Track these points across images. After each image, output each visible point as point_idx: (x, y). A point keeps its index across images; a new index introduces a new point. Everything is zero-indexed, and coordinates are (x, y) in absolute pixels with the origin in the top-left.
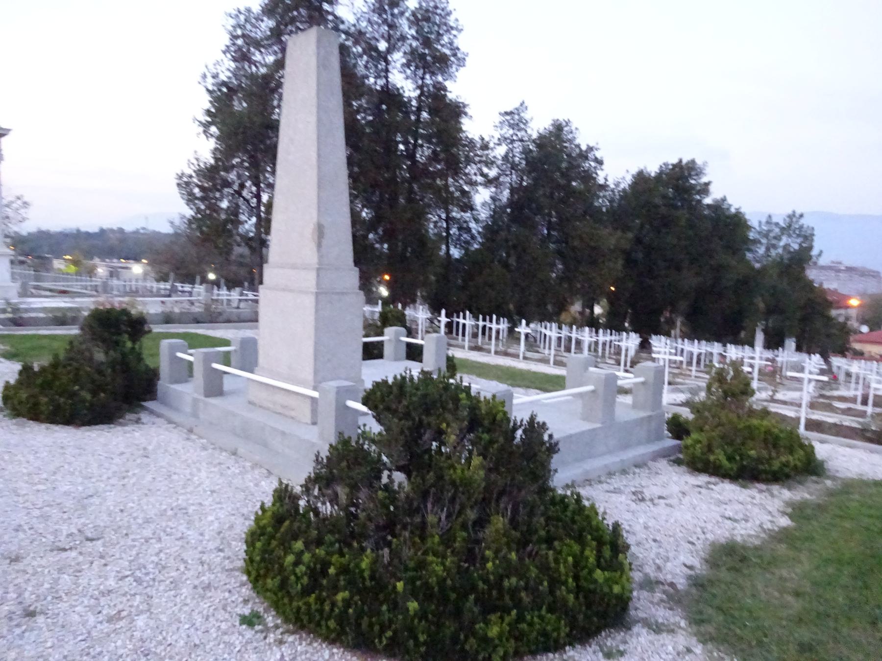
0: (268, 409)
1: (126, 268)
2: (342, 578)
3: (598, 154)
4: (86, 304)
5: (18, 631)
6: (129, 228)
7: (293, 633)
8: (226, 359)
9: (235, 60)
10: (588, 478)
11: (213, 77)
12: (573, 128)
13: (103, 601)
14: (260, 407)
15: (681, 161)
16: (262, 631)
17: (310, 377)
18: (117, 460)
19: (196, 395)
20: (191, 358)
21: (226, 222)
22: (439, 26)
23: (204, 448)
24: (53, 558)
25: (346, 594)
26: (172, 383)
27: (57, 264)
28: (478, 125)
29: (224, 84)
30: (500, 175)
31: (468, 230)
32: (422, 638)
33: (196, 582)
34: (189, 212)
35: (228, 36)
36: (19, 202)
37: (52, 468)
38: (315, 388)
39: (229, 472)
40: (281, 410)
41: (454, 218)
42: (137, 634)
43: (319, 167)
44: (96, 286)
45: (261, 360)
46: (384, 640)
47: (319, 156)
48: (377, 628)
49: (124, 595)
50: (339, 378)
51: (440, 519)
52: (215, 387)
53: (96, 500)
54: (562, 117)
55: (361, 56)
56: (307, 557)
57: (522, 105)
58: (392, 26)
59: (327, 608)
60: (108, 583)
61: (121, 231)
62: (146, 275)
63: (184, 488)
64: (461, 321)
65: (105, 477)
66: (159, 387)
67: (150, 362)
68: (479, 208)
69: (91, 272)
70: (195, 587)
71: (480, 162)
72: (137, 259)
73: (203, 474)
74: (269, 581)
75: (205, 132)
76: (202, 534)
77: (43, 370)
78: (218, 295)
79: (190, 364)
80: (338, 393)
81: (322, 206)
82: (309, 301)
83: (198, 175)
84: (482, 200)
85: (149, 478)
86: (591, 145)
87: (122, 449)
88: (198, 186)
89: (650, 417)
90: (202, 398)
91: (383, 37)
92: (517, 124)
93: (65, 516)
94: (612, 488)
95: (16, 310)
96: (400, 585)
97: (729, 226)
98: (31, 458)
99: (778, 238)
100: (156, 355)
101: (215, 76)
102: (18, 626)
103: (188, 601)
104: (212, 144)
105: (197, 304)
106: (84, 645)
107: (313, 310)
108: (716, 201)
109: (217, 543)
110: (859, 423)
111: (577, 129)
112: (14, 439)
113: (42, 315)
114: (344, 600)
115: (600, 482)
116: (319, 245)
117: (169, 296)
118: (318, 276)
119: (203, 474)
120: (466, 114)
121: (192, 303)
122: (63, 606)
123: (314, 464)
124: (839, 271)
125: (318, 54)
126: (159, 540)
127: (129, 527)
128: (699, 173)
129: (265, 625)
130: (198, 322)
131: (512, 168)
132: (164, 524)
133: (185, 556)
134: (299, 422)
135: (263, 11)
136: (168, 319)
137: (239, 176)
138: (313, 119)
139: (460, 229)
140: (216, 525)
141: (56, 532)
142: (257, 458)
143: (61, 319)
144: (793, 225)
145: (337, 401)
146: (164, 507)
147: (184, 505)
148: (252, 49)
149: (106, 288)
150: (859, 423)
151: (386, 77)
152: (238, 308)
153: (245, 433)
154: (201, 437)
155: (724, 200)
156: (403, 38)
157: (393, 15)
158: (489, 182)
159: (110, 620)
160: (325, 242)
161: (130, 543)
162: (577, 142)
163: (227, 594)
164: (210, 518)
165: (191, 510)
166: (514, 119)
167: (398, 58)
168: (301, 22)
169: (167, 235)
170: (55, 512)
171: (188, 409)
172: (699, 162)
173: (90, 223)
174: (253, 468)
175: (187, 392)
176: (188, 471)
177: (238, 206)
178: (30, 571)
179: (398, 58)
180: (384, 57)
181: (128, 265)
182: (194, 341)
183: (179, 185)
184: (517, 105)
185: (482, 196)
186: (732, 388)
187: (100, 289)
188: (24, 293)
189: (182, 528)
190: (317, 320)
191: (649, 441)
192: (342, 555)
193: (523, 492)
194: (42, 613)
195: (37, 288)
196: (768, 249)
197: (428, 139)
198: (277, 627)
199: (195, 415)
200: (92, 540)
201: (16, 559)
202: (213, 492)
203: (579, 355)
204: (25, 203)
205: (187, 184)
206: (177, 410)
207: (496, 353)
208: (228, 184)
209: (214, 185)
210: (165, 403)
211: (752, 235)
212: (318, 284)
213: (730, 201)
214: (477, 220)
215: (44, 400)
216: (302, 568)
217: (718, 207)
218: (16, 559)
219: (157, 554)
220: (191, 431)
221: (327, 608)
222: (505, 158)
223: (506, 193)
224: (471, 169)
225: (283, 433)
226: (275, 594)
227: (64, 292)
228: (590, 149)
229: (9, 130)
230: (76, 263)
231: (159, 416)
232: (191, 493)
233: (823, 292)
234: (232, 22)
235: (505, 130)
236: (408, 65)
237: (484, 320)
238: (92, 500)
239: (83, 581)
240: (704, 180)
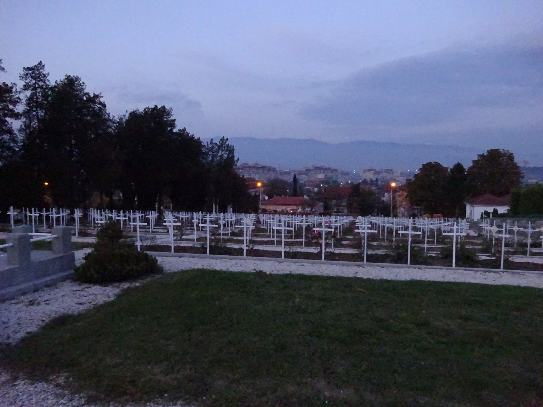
3: (102, 100)
12: (81, 82)
15: (156, 107)
54: (73, 74)
57: (39, 64)
64: (29, 214)
68: (16, 132)
86: (97, 94)
89: (62, 257)
92: (39, 77)
97: (188, 144)
99: (218, 151)
108: (180, 130)
110: (434, 254)
111: (83, 83)
124: (259, 168)
128: (168, 114)
144: (223, 144)
150: (434, 254)
155: (184, 130)
158: (17, 116)
162: (86, 91)
166: (35, 73)
172: (168, 107)
186: (112, 233)
191: (61, 270)
196: (213, 158)
203: (58, 227)
211: (204, 150)
213: (188, 131)
217: (183, 134)
222: (30, 99)
228: (96, 96)
233: (243, 179)
240: (172, 118)
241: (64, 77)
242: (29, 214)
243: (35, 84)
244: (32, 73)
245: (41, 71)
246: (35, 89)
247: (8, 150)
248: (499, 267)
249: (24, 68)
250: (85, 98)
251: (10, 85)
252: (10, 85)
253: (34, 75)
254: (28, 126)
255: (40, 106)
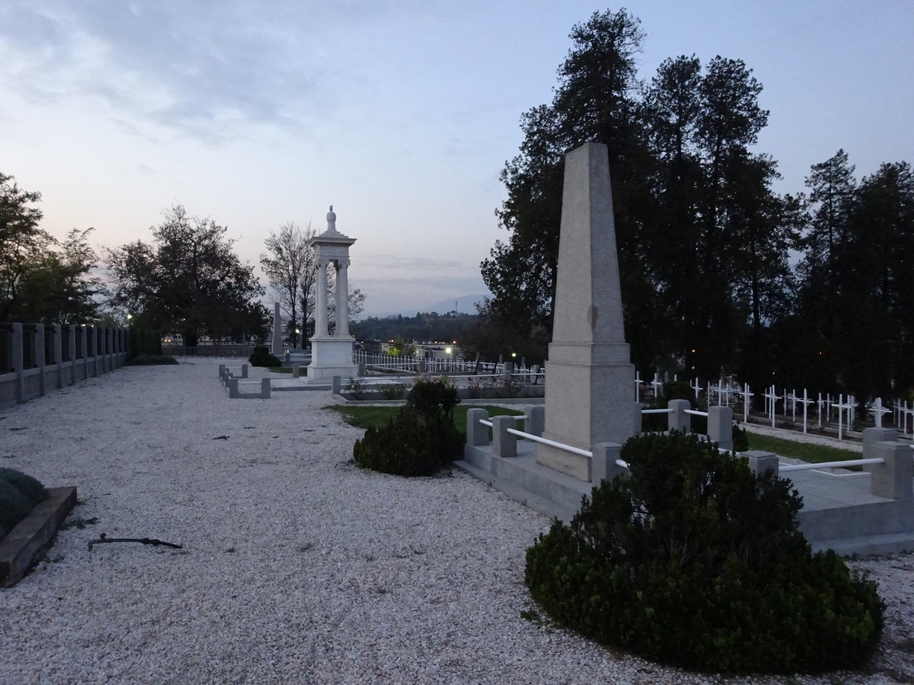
0: (553, 469)
1: (439, 349)
2: (595, 585)
4: (409, 381)
5: (375, 600)
6: (441, 312)
7: (558, 628)
8: (520, 426)
9: (531, 154)
10: (874, 553)
11: (513, 173)
13: (427, 591)
14: (547, 466)
16: (537, 624)
17: (587, 439)
18: (435, 502)
19: (495, 456)
20: (491, 424)
21: (526, 302)
22: (734, 90)
23: (500, 498)
24: (394, 561)
25: (598, 597)
26: (476, 445)
27: (385, 348)
28: (789, 182)
29: (522, 177)
30: (816, 234)
31: (781, 296)
32: (657, 638)
33: (491, 588)
34: (492, 297)
35: (524, 135)
36: (357, 296)
37: (390, 503)
38: (591, 450)
39: (520, 518)
40: (562, 469)
41: (763, 284)
42: (450, 612)
43: (592, 260)
44: (415, 366)
45: (548, 425)
46: (627, 636)
47: (592, 248)
48: (621, 626)
49: (442, 589)
50: (612, 441)
51: (681, 552)
52: (510, 448)
53: (421, 528)
55: (652, 132)
56: (570, 568)
57: (839, 155)
58: (683, 98)
59: (584, 607)
60: (430, 580)
61: (434, 315)
62: (455, 353)
63: (484, 525)
65: (426, 513)
66: (466, 450)
67: (459, 429)
68: (793, 271)
69: (411, 353)
70: (490, 590)
71: (788, 223)
72: (449, 342)
73: (499, 518)
74: (542, 586)
75: (505, 222)
76: (496, 558)
77: (382, 431)
78: (519, 372)
79: (490, 428)
80: (608, 452)
81: (595, 292)
82: (586, 373)
83: (499, 262)
84: (796, 262)
85: (459, 516)
87: (438, 495)
88: (499, 271)
90: (499, 457)
91: (674, 110)
93: (401, 536)
94: (901, 565)
95: (357, 387)
96: (640, 594)
98: (376, 496)
100: (465, 424)
101: (515, 172)
102: (375, 597)
103: (485, 598)
104: (512, 232)
105: (499, 381)
106: (415, 613)
107: (589, 381)
109: (508, 565)
112: (363, 483)
113: (375, 391)
114: (596, 601)
115: (889, 559)
116: (594, 325)
117: (475, 373)
118: (593, 351)
119: (499, 518)
120: (773, 172)
121: (494, 379)
122: (402, 590)
123: (580, 505)
125: (590, 165)
126: (465, 558)
127: (444, 548)
129: (540, 621)
130: (500, 397)
131: (831, 225)
132: (469, 548)
133: (483, 570)
134: (579, 480)
135: (555, 107)
136: (474, 394)
137: (537, 260)
138: (587, 218)
139: (769, 296)
140: (507, 554)
141: (395, 546)
142: (543, 508)
143: (390, 393)
145: (608, 461)
146: (469, 537)
147: (484, 537)
148: (547, 143)
149: (423, 368)
151: (679, 149)
152: (535, 384)
153: (534, 487)
154: (498, 490)
156: (695, 109)
157: (683, 87)
158: (799, 244)
159: (432, 602)
160: (599, 322)
161: (444, 558)
163: (513, 598)
164: (503, 548)
165: (488, 541)
167: (690, 128)
168: (591, 111)
169: (474, 316)
170: (394, 533)
171: (489, 467)
173: (409, 310)
174: (539, 516)
175: (489, 452)
176: (487, 514)
177: (536, 289)
178: (380, 567)
179: (690, 128)
180: (676, 129)
181: (441, 347)
182: (492, 412)
183: (483, 272)
184: (834, 155)
185: (795, 258)
187: (419, 368)
188: (362, 374)
189: (482, 552)
190: (592, 391)
192: (597, 569)
193: (474, 366)
194: (389, 592)
195: (370, 368)
197: (728, 204)
198: (548, 622)
199: (494, 472)
200: (419, 553)
201: (371, 559)
202: (506, 530)
204: (361, 296)
205: (491, 270)
206: (480, 468)
207: (809, 431)
208: (527, 268)
209: (514, 270)
210: (470, 462)
212: (593, 358)
214: (791, 286)
215: (383, 454)
216: (565, 577)
218: (371, 559)
219: (464, 567)
220: (490, 485)
221: (584, 607)
222: (822, 214)
223: (825, 254)
224: (780, 230)
225: (564, 488)
226: (547, 597)
227: (391, 372)
229: (355, 240)
230: (399, 346)
231: (466, 472)
232: (489, 530)
234: (528, 121)
235: (820, 185)
236: (701, 134)
237: (824, 398)
238: (418, 528)
239: (414, 577)
241: (879, 168)
242: (900, 409)
243: (829, 189)
244: (826, 172)
245: (841, 165)
246: (830, 196)
247: (779, 300)
248: (543, 410)
249: (813, 167)
250: (130, 317)
251: (795, 197)
252: (795, 197)
253: (828, 174)
254: (811, 259)
255: (834, 222)
